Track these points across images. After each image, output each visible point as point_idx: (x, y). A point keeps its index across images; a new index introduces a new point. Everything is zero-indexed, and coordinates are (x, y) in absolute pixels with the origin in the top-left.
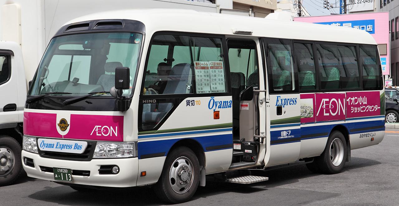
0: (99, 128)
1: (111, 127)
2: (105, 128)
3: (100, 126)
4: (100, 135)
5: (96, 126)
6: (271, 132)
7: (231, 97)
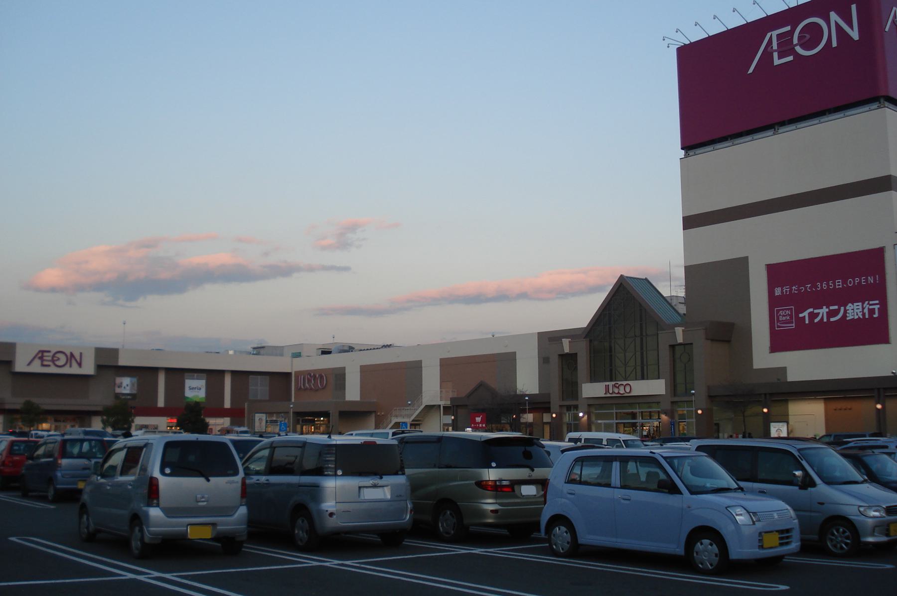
1: (834, 16)
4: (791, 58)
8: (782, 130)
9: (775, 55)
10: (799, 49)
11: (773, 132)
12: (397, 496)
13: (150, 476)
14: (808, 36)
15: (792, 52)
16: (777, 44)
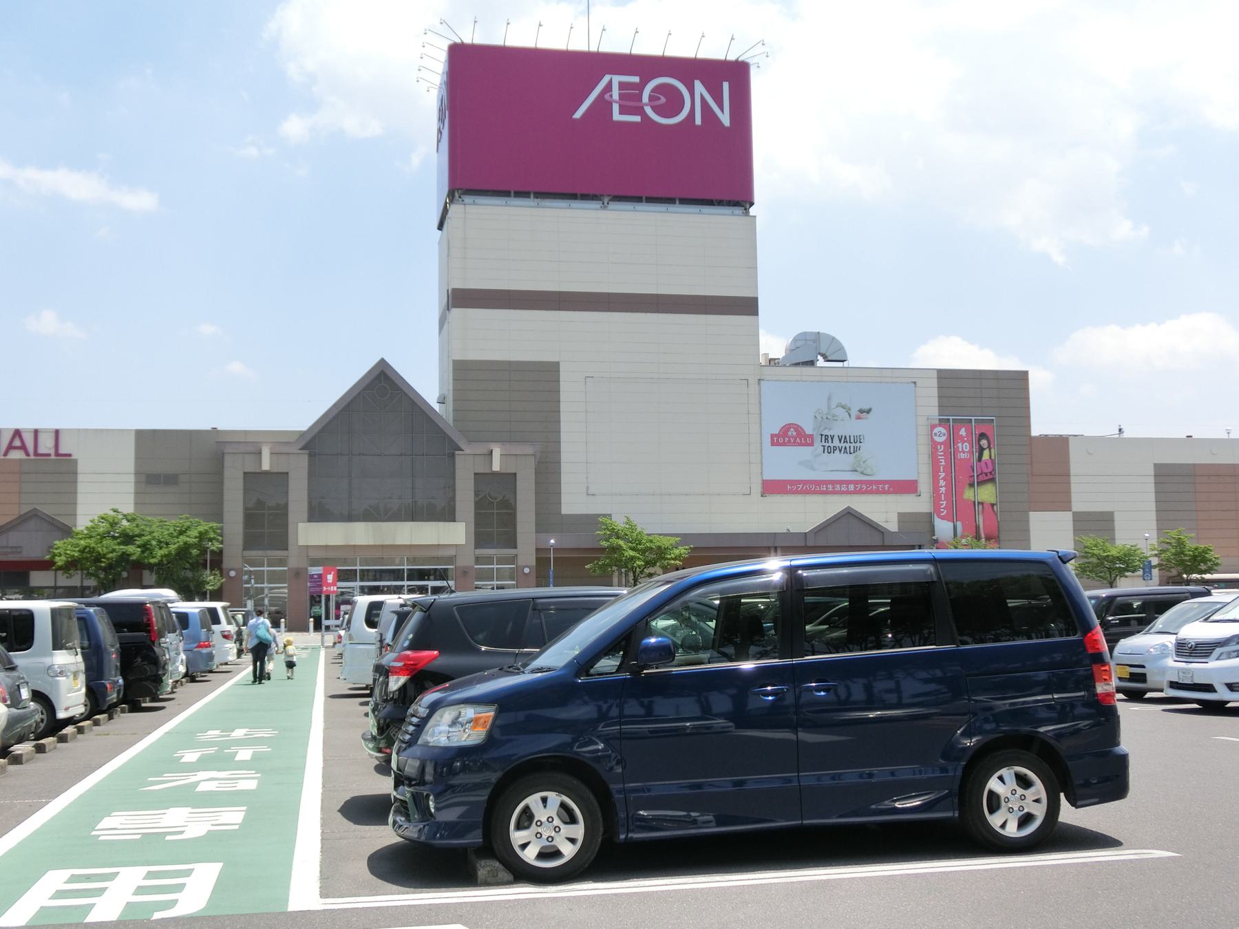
0: (622, 86)
1: (699, 87)
2: (659, 89)
3: (636, 79)
4: (637, 119)
5: (606, 78)
6: (432, 594)
7: (724, 83)
8: (614, 205)
9: (616, 108)
10: (648, 110)
11: (600, 205)
12: (163, 708)
13: (154, 573)
14: (663, 100)
15: (639, 111)
16: (612, 91)
